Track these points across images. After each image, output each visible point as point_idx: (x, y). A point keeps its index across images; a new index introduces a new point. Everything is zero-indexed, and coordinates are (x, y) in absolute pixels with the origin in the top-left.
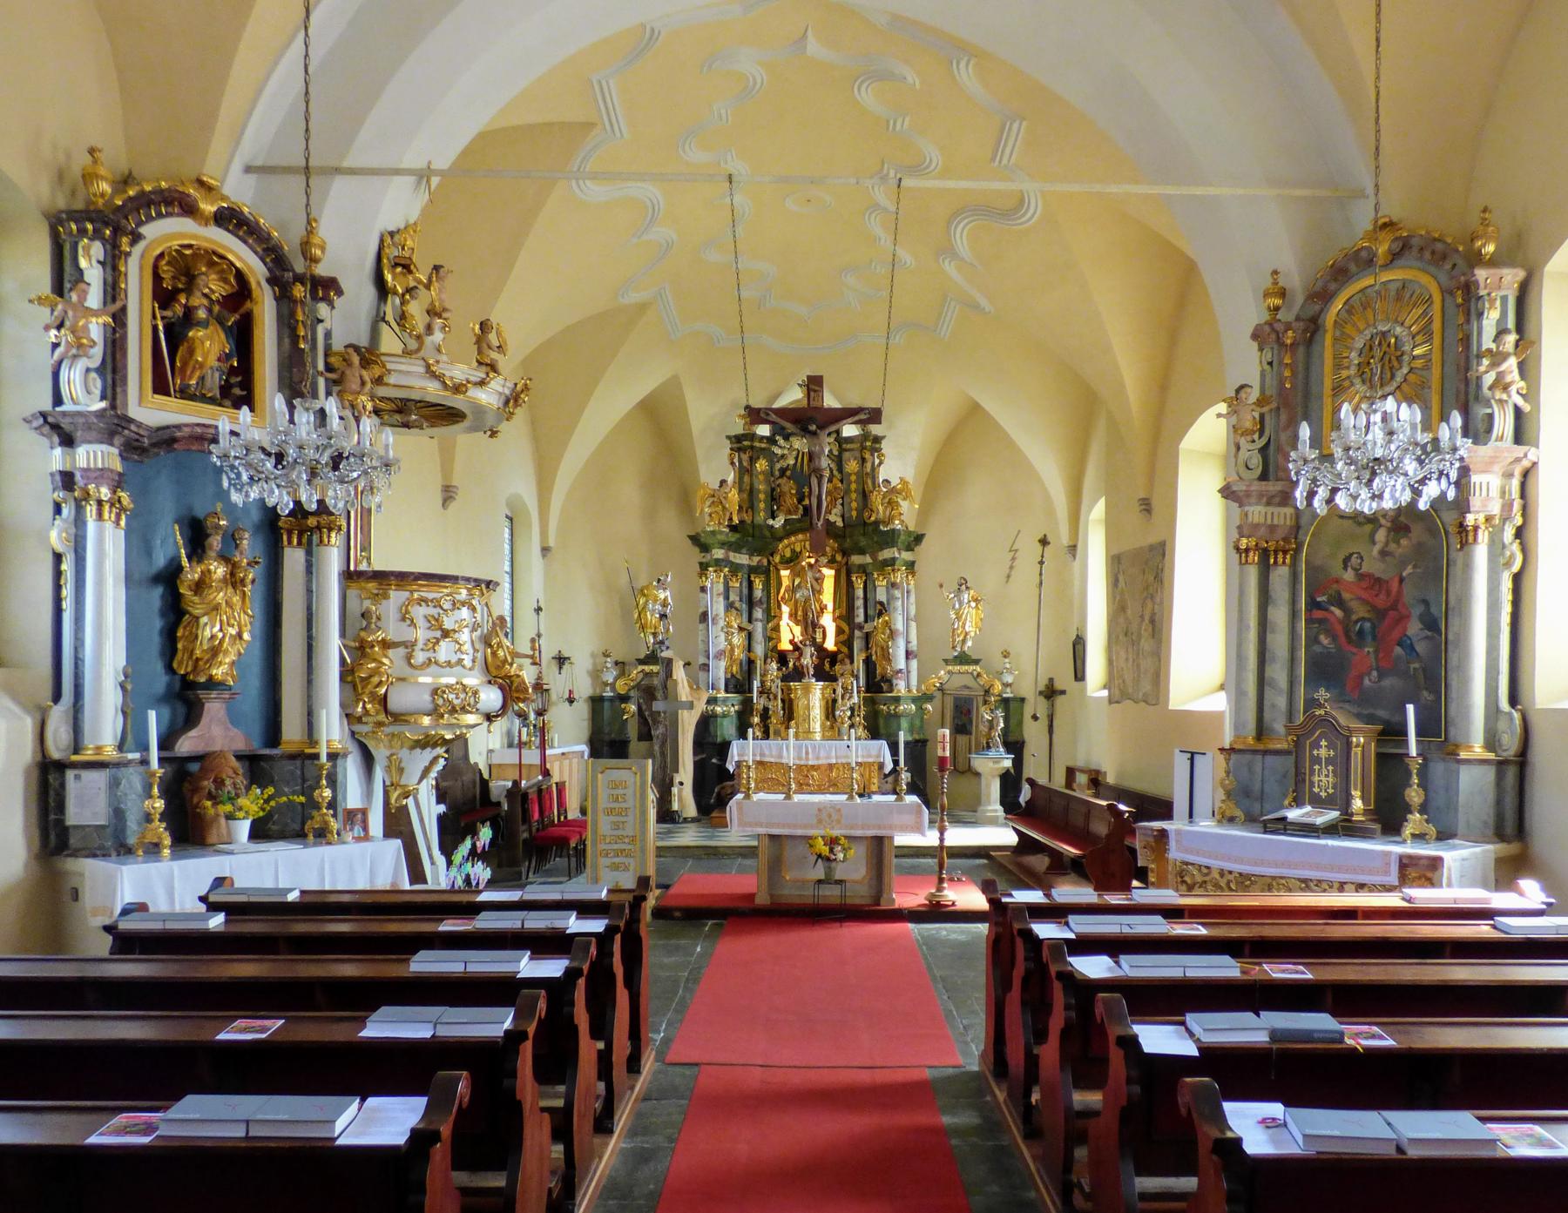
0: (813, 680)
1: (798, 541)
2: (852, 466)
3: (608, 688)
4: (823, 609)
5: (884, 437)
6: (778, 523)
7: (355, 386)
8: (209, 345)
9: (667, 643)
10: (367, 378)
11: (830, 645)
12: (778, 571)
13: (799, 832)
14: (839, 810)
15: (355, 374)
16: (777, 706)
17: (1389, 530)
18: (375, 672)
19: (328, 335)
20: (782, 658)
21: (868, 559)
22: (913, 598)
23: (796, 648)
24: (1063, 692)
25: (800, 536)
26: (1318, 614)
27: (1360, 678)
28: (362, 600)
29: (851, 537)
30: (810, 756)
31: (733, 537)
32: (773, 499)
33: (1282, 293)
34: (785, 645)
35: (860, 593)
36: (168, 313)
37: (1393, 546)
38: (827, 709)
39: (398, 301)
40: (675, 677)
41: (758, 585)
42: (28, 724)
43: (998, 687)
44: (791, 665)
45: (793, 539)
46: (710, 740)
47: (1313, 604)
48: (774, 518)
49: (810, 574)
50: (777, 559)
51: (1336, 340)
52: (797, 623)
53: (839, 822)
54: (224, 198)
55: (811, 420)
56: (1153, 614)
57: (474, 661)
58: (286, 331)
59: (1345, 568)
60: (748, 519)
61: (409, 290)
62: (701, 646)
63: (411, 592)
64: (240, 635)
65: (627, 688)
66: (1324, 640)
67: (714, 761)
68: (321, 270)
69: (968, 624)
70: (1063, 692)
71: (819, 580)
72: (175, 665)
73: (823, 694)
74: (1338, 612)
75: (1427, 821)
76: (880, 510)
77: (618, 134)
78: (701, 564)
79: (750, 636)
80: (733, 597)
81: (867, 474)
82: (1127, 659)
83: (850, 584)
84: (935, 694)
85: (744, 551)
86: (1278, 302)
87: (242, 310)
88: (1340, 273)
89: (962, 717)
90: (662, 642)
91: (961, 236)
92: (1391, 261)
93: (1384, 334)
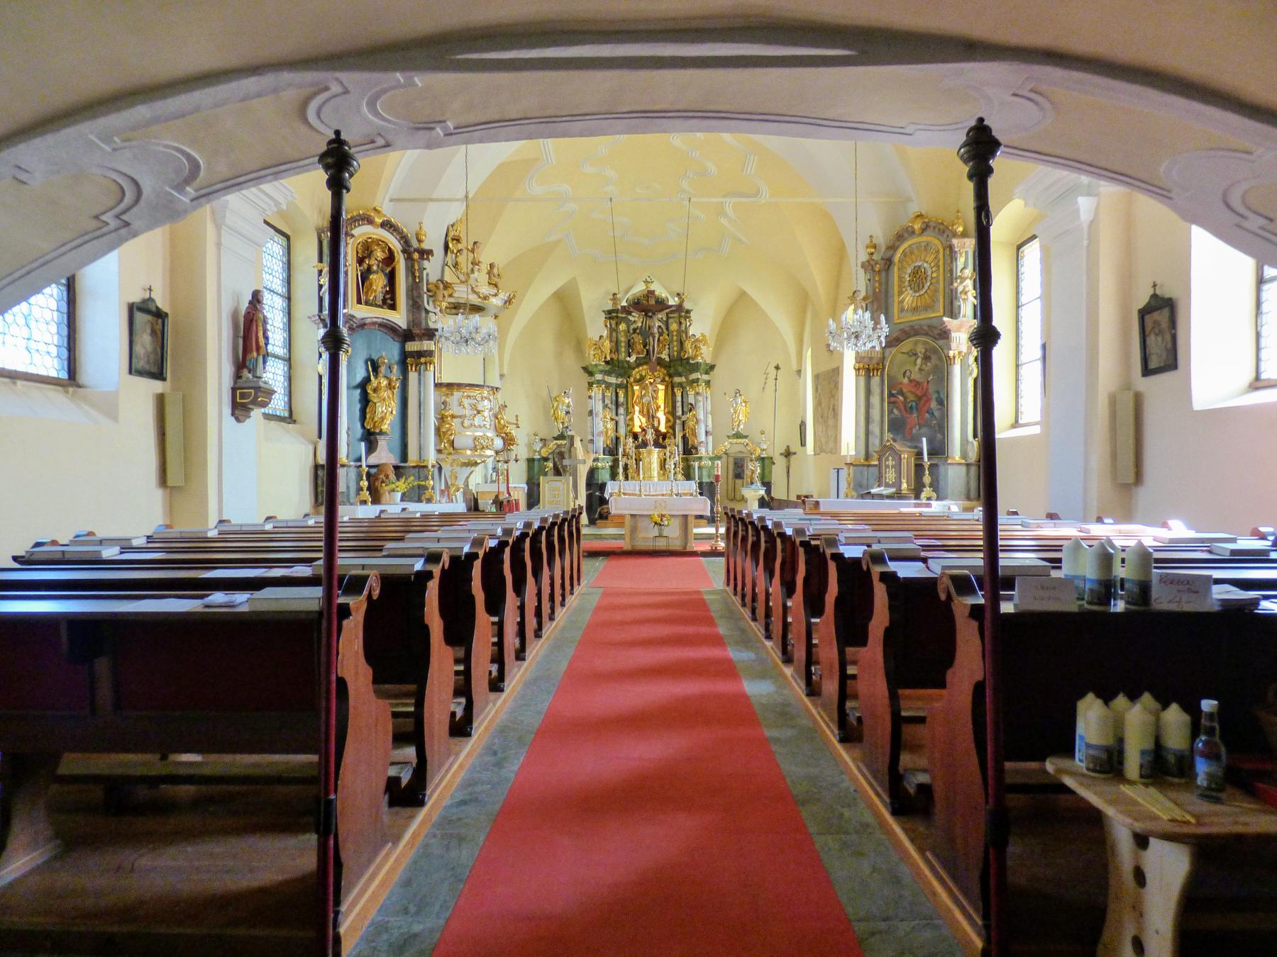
0: (653, 448)
1: (643, 370)
2: (674, 327)
3: (537, 454)
4: (658, 407)
5: (692, 310)
6: (632, 359)
7: (441, 298)
8: (378, 282)
9: (570, 428)
10: (446, 295)
11: (663, 429)
12: (632, 386)
13: (645, 513)
14: (665, 502)
15: (440, 293)
16: (632, 463)
17: (923, 359)
18: (449, 429)
19: (427, 275)
20: (635, 436)
21: (683, 379)
22: (709, 402)
23: (643, 430)
24: (795, 453)
25: (645, 367)
26: (893, 399)
27: (911, 429)
28: (441, 396)
29: (674, 367)
30: (652, 490)
31: (608, 368)
32: (629, 346)
33: (875, 247)
34: (637, 429)
35: (679, 398)
36: (362, 268)
37: (924, 366)
38: (661, 464)
39: (454, 256)
40: (575, 446)
41: (621, 394)
42: (311, 448)
43: (758, 451)
44: (640, 440)
45: (641, 368)
46: (595, 482)
47: (891, 395)
48: (630, 356)
49: (650, 388)
50: (632, 380)
51: (899, 269)
52: (643, 416)
53: (665, 507)
54: (385, 216)
55: (650, 311)
56: (834, 405)
57: (490, 425)
58: (410, 275)
59: (904, 377)
60: (615, 357)
61: (459, 251)
62: (589, 430)
63: (464, 392)
64: (392, 412)
65: (548, 453)
66: (896, 411)
67: (597, 494)
68: (425, 246)
69: (741, 415)
70: (795, 453)
71: (656, 391)
72: (365, 425)
73: (658, 455)
74: (901, 398)
75: (933, 491)
76: (690, 350)
77: (550, 162)
78: (589, 383)
79: (617, 423)
80: (607, 401)
81: (683, 331)
82: (822, 431)
83: (674, 394)
84: (723, 455)
85: (613, 375)
86: (873, 250)
87: (392, 266)
88: (900, 237)
89: (738, 470)
90: (567, 427)
91: (729, 207)
92: (922, 233)
93: (919, 267)
